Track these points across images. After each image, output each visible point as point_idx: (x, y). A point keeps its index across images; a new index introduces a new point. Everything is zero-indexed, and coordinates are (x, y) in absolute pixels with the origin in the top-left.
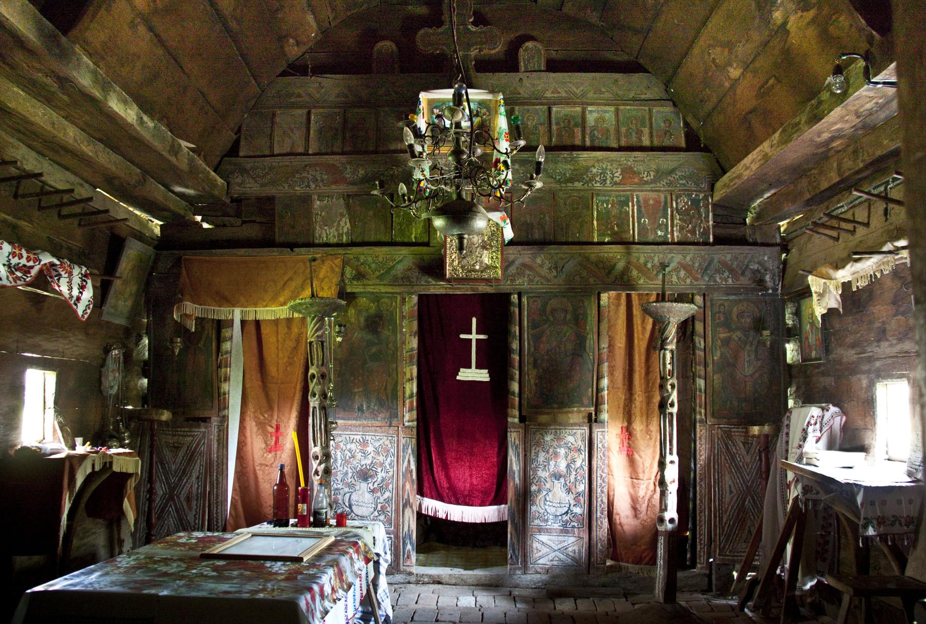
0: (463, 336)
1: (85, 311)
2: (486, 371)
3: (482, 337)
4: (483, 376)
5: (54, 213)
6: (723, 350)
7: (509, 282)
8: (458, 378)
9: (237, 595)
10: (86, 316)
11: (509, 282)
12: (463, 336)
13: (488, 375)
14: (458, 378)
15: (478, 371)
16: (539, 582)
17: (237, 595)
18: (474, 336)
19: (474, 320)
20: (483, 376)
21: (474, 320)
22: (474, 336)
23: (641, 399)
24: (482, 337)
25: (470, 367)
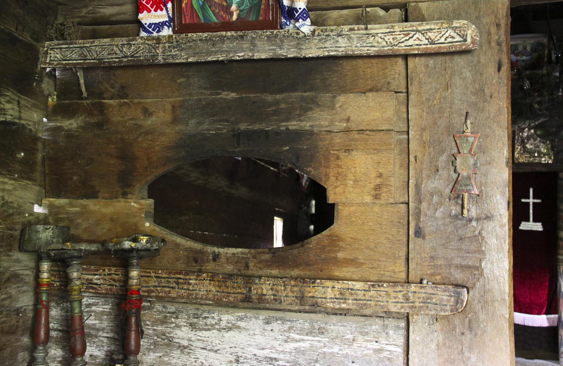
0: (523, 200)
1: (305, 183)
2: (540, 224)
3: (536, 201)
4: (538, 227)
5: (352, 126)
6: (50, 151)
7: (558, 164)
8: (520, 228)
9: (134, 328)
10: (306, 186)
11: (558, 164)
12: (523, 200)
13: (541, 227)
14: (520, 228)
15: (534, 224)
16: (442, 334)
17: (134, 328)
18: (531, 201)
19: (531, 190)
20: (538, 227)
21: (531, 190)
22: (531, 201)
23: (61, 202)
24: (536, 201)
25: (528, 220)
